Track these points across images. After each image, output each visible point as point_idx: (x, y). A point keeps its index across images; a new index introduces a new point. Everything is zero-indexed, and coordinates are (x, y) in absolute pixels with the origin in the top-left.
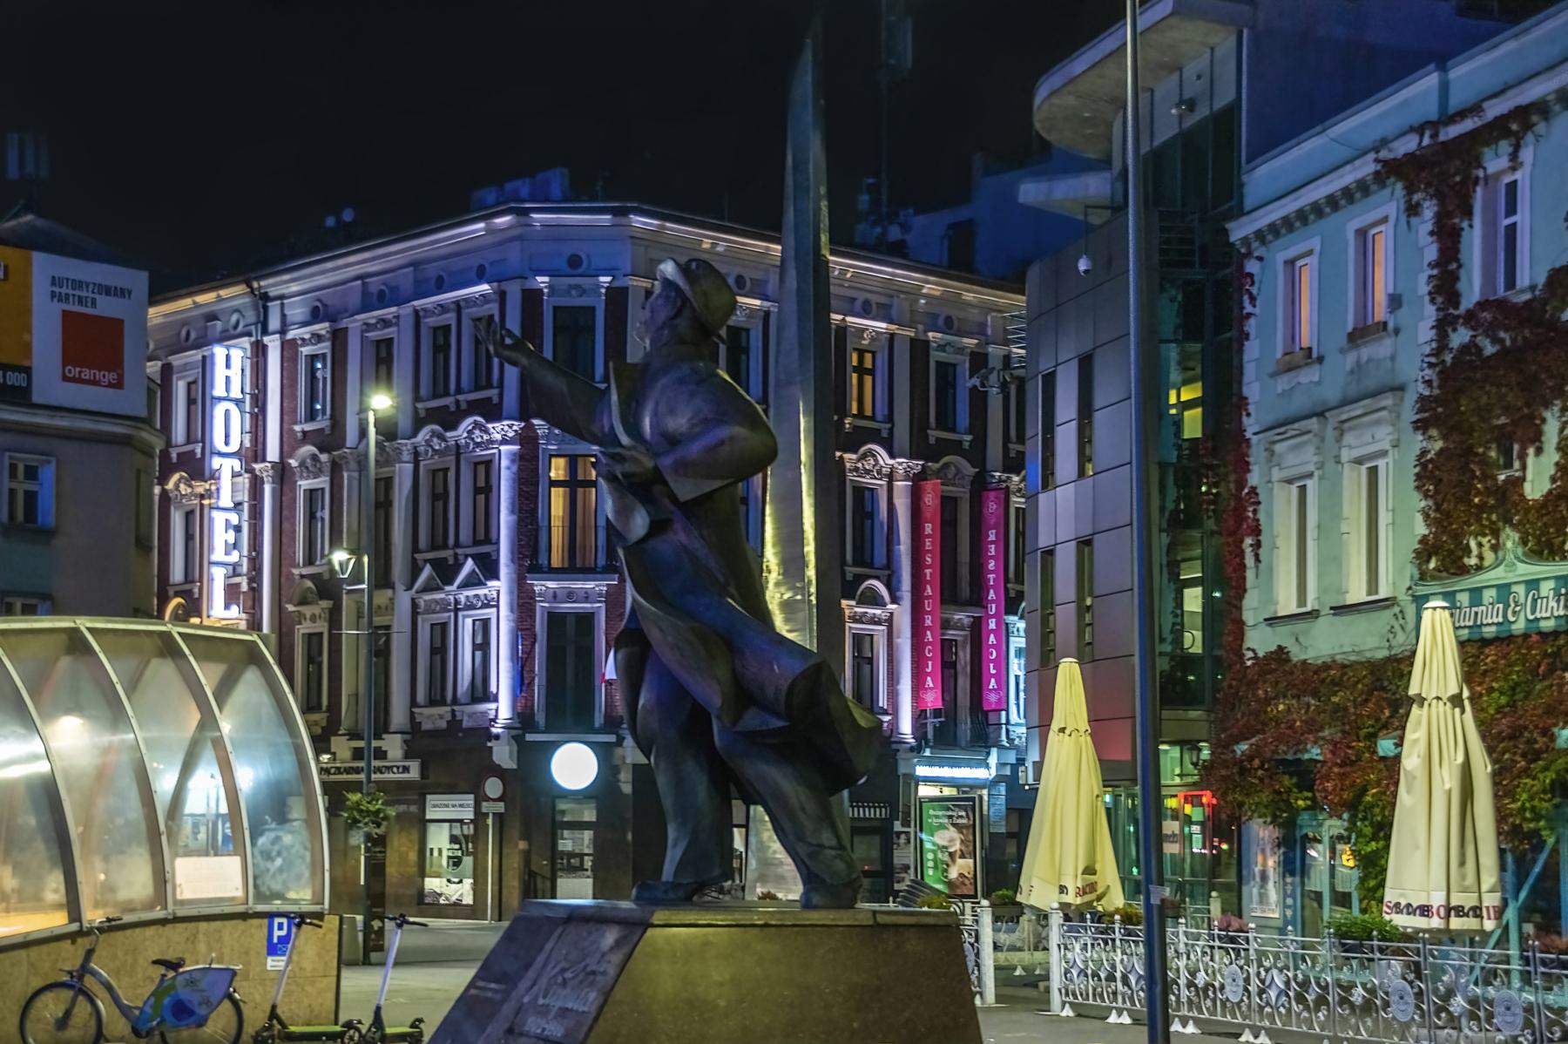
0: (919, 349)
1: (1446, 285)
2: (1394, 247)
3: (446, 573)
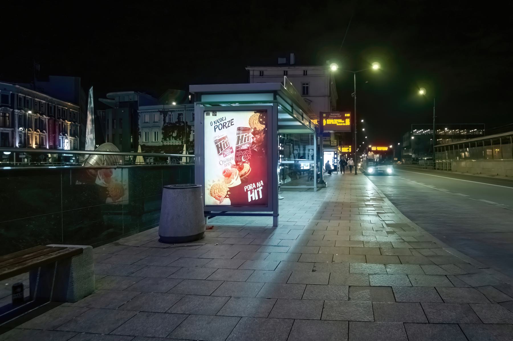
0: (48, 104)
1: (164, 120)
2: (158, 117)
3: (347, 163)
